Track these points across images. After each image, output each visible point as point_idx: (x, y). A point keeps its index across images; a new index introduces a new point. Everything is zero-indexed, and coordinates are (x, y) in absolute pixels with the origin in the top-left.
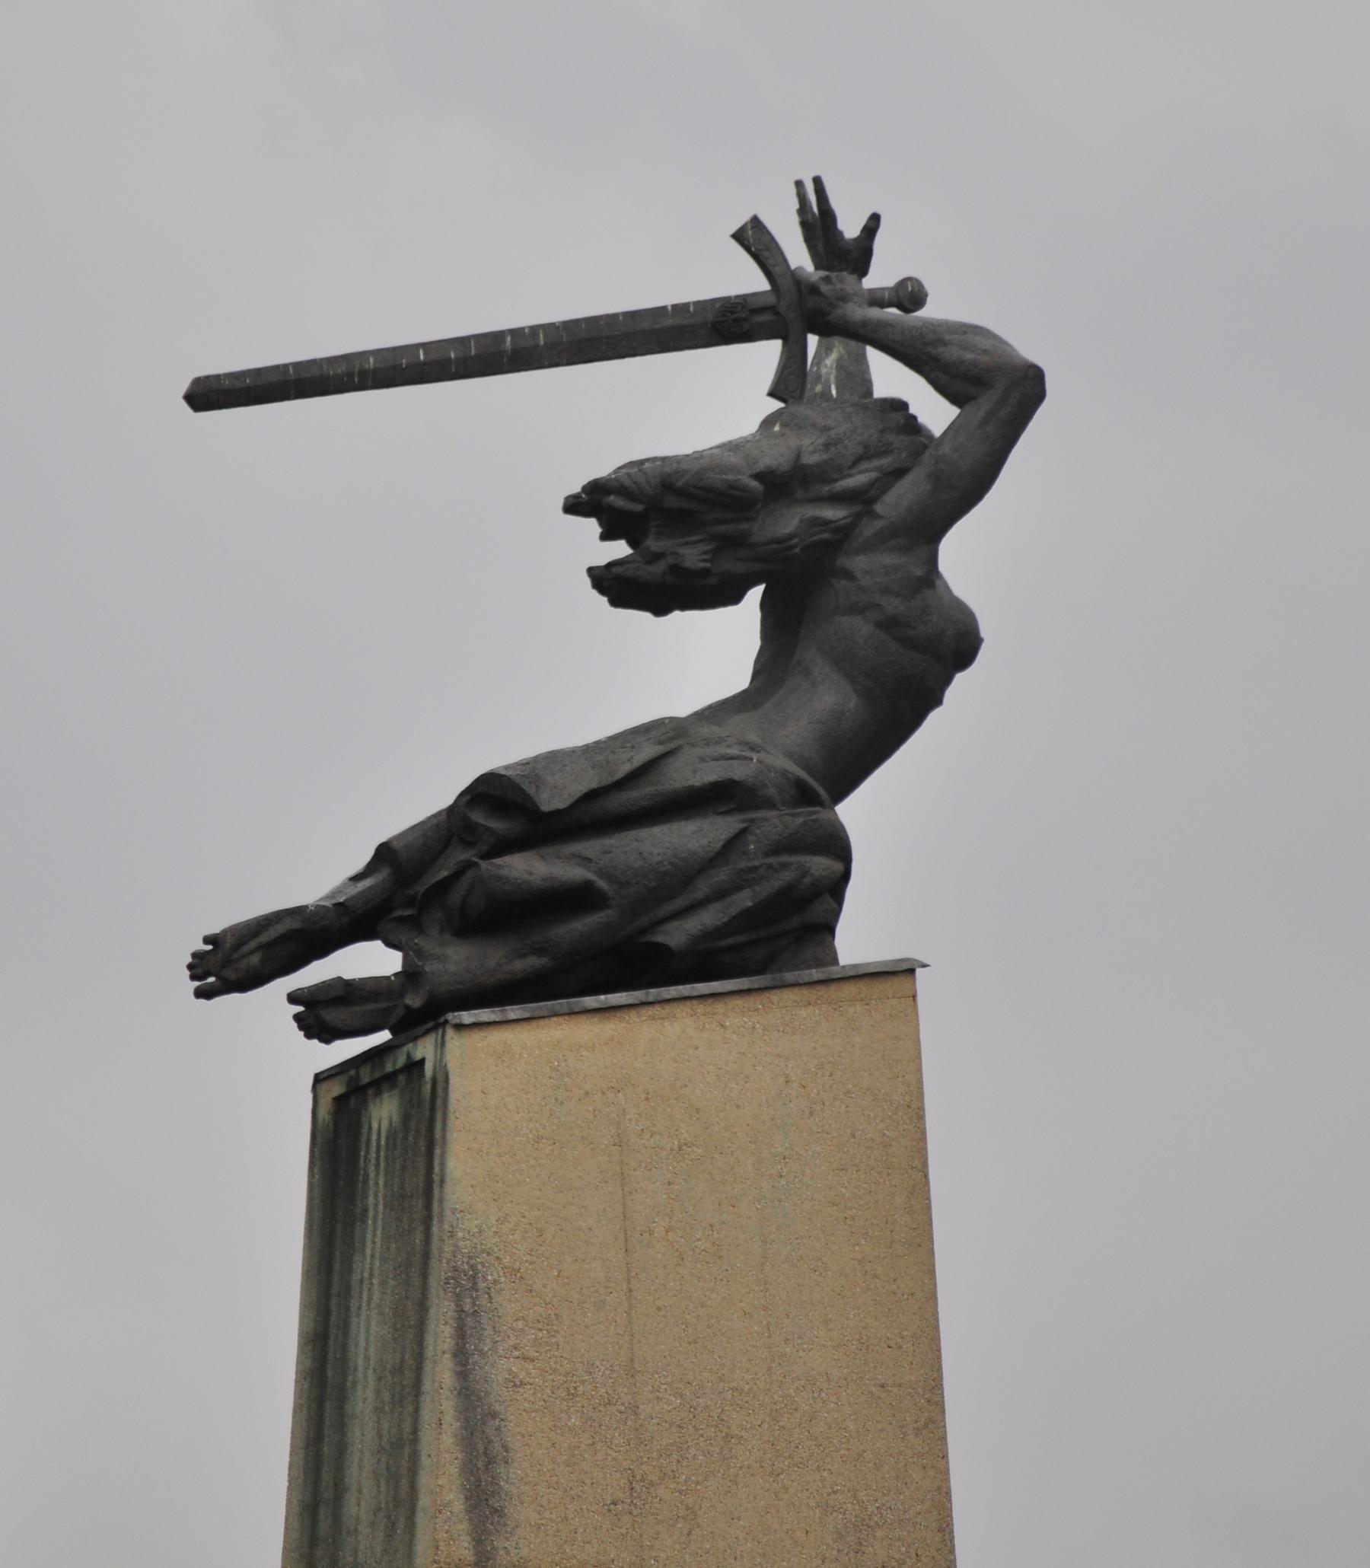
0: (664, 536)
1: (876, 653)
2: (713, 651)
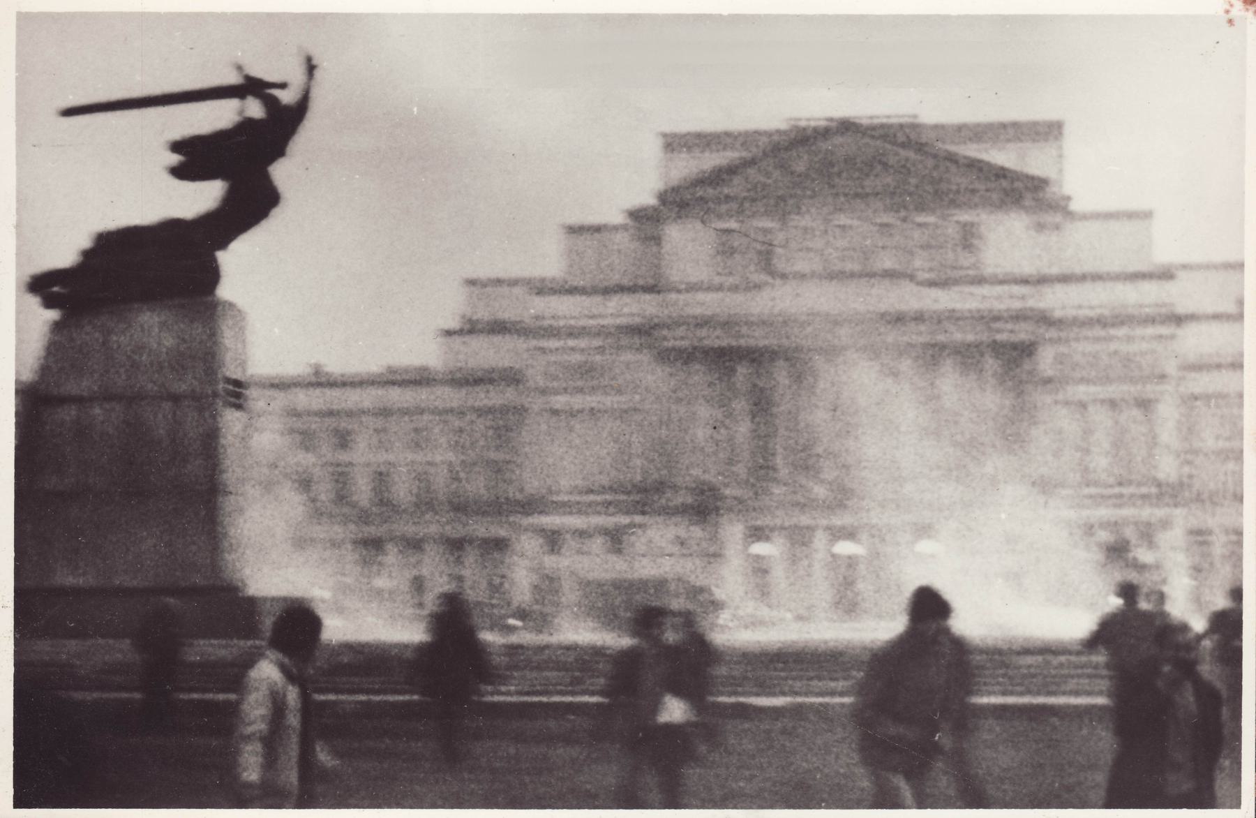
0: (195, 159)
1: (251, 203)
2: (203, 197)
